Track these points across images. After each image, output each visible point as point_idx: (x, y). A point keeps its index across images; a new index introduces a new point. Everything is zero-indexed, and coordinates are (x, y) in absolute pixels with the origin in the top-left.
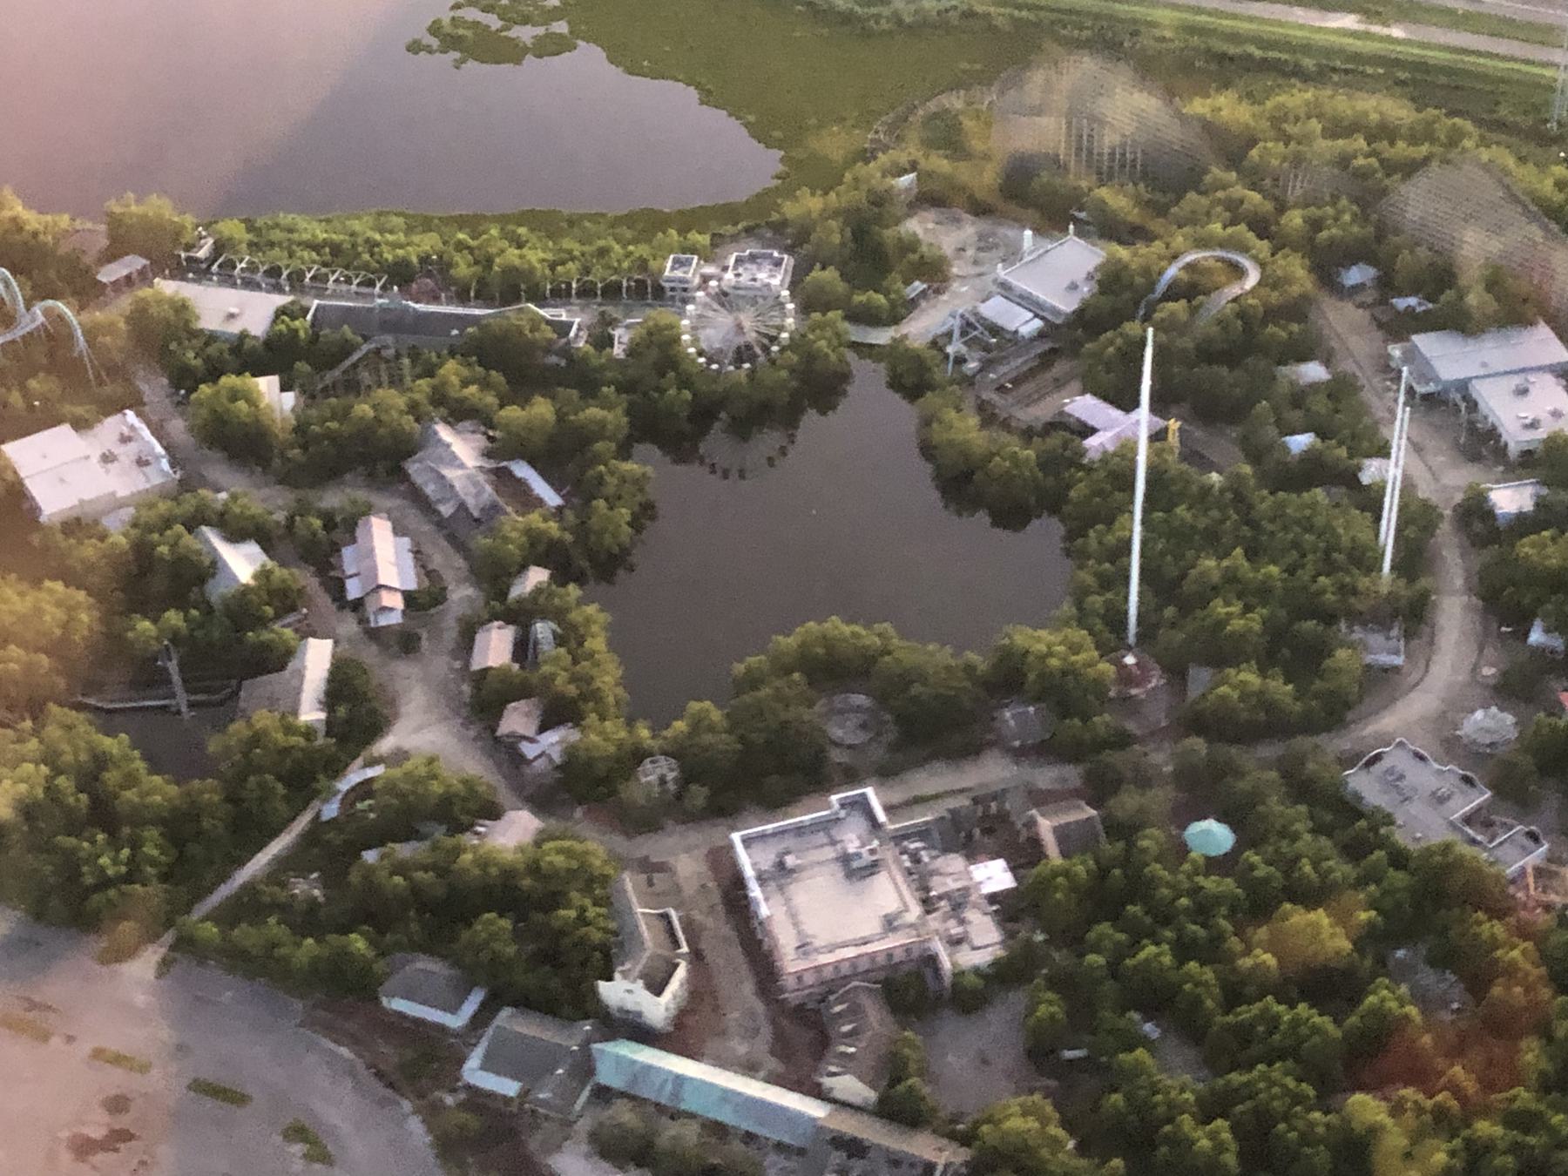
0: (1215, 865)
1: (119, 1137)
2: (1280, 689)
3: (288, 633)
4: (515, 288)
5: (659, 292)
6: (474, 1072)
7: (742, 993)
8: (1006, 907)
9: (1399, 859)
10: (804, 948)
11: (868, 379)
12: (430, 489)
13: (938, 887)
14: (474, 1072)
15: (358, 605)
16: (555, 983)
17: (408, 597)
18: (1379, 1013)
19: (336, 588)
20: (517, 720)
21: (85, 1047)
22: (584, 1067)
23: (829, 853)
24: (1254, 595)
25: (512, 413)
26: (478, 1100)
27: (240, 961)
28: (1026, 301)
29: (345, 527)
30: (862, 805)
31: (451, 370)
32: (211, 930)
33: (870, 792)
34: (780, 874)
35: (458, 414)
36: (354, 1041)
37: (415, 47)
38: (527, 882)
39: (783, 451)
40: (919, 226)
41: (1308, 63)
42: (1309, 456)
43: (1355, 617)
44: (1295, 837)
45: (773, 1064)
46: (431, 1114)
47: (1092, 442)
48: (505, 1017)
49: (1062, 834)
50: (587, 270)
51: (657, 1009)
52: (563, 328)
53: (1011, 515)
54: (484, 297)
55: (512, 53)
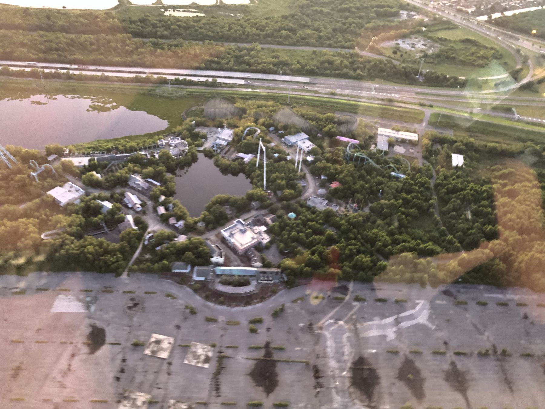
0: (296, 219)
1: (136, 305)
2: (293, 191)
3: (123, 215)
4: (132, 150)
5: (158, 146)
6: (195, 277)
7: (232, 256)
8: (267, 232)
9: (320, 213)
10: (242, 245)
11: (201, 156)
12: (135, 186)
13: (256, 231)
14: (195, 277)
15: (132, 208)
16: (203, 260)
17: (141, 205)
18: (329, 234)
19: (126, 206)
20: (172, 221)
21: (121, 291)
22: (214, 272)
23: (238, 230)
24: (282, 179)
25: (144, 171)
26: (197, 282)
27: (142, 271)
28: (224, 140)
30: (239, 222)
31: (130, 165)
32: (135, 267)
33: (240, 220)
34: (232, 235)
35: (134, 172)
36: (170, 279)
37: (88, 110)
38: (190, 246)
39: (187, 171)
40: (197, 130)
41: (248, 97)
42: (279, 157)
43: (297, 179)
44: (304, 213)
45: (242, 264)
46: (190, 286)
47: (245, 160)
48: (196, 268)
49: (271, 219)
50: (144, 145)
51: (221, 260)
52: (146, 155)
53: (235, 174)
54: (127, 152)
55: (108, 109)
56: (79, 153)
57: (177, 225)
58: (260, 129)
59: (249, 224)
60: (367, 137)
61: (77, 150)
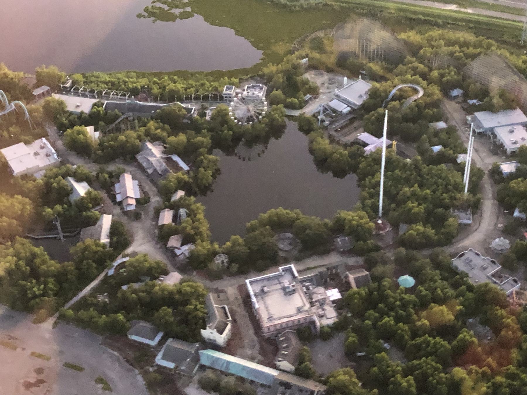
1: (40, 382)
2: (430, 231)
3: (97, 213)
4: (173, 97)
5: (221, 98)
6: (159, 360)
7: (249, 334)
8: (338, 305)
9: (470, 289)
10: (270, 318)
11: (292, 127)
12: (144, 164)
13: (315, 298)
14: (159, 360)
15: (120, 203)
16: (187, 330)
17: (137, 200)
18: (463, 340)
19: (113, 198)
20: (174, 242)
21: (29, 352)
22: (196, 358)
23: (279, 286)
24: (421, 200)
25: (172, 139)
26: (161, 369)
27: (81, 323)
29: (116, 177)
30: (290, 270)
31: (152, 124)
32: (71, 312)
34: (262, 294)
35: (154, 139)
36: (119, 350)
37: (139, 16)
38: (177, 296)
39: (263, 152)
40: (309, 76)
41: (440, 21)
42: (440, 153)
43: (455, 207)
44: (435, 281)
45: (260, 357)
46: (145, 374)
47: (367, 148)
48: (170, 342)
49: (357, 280)
50: (197, 91)
51: (221, 339)
52: (189, 110)
53: (340, 173)
54: (163, 100)
55: (172, 18)
56: (85, 90)
57: (178, 252)
58: (424, 89)
59: (310, 280)
60: (380, 153)
61: (85, 83)
